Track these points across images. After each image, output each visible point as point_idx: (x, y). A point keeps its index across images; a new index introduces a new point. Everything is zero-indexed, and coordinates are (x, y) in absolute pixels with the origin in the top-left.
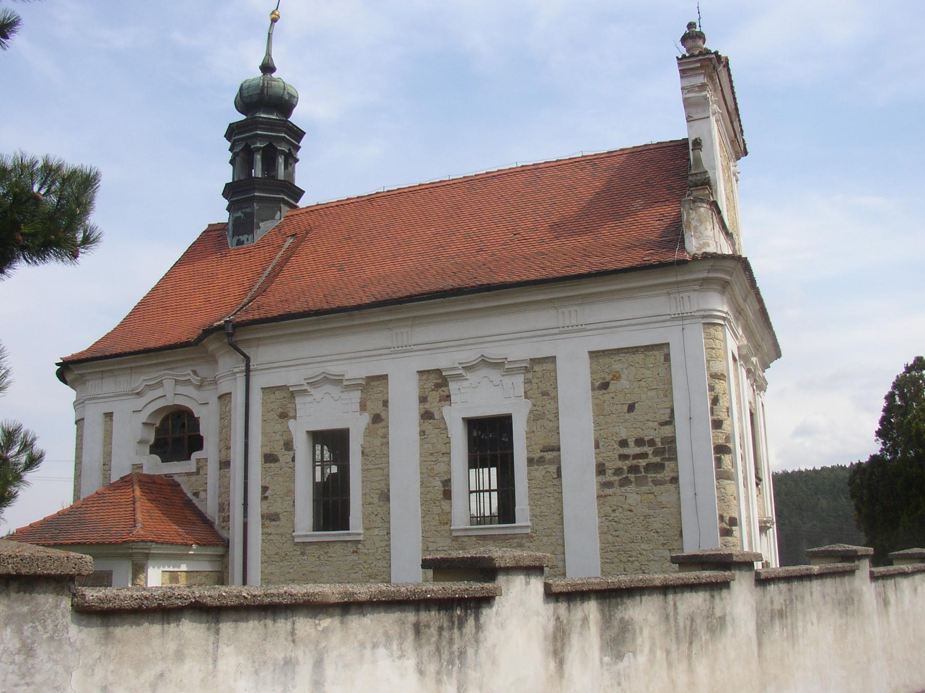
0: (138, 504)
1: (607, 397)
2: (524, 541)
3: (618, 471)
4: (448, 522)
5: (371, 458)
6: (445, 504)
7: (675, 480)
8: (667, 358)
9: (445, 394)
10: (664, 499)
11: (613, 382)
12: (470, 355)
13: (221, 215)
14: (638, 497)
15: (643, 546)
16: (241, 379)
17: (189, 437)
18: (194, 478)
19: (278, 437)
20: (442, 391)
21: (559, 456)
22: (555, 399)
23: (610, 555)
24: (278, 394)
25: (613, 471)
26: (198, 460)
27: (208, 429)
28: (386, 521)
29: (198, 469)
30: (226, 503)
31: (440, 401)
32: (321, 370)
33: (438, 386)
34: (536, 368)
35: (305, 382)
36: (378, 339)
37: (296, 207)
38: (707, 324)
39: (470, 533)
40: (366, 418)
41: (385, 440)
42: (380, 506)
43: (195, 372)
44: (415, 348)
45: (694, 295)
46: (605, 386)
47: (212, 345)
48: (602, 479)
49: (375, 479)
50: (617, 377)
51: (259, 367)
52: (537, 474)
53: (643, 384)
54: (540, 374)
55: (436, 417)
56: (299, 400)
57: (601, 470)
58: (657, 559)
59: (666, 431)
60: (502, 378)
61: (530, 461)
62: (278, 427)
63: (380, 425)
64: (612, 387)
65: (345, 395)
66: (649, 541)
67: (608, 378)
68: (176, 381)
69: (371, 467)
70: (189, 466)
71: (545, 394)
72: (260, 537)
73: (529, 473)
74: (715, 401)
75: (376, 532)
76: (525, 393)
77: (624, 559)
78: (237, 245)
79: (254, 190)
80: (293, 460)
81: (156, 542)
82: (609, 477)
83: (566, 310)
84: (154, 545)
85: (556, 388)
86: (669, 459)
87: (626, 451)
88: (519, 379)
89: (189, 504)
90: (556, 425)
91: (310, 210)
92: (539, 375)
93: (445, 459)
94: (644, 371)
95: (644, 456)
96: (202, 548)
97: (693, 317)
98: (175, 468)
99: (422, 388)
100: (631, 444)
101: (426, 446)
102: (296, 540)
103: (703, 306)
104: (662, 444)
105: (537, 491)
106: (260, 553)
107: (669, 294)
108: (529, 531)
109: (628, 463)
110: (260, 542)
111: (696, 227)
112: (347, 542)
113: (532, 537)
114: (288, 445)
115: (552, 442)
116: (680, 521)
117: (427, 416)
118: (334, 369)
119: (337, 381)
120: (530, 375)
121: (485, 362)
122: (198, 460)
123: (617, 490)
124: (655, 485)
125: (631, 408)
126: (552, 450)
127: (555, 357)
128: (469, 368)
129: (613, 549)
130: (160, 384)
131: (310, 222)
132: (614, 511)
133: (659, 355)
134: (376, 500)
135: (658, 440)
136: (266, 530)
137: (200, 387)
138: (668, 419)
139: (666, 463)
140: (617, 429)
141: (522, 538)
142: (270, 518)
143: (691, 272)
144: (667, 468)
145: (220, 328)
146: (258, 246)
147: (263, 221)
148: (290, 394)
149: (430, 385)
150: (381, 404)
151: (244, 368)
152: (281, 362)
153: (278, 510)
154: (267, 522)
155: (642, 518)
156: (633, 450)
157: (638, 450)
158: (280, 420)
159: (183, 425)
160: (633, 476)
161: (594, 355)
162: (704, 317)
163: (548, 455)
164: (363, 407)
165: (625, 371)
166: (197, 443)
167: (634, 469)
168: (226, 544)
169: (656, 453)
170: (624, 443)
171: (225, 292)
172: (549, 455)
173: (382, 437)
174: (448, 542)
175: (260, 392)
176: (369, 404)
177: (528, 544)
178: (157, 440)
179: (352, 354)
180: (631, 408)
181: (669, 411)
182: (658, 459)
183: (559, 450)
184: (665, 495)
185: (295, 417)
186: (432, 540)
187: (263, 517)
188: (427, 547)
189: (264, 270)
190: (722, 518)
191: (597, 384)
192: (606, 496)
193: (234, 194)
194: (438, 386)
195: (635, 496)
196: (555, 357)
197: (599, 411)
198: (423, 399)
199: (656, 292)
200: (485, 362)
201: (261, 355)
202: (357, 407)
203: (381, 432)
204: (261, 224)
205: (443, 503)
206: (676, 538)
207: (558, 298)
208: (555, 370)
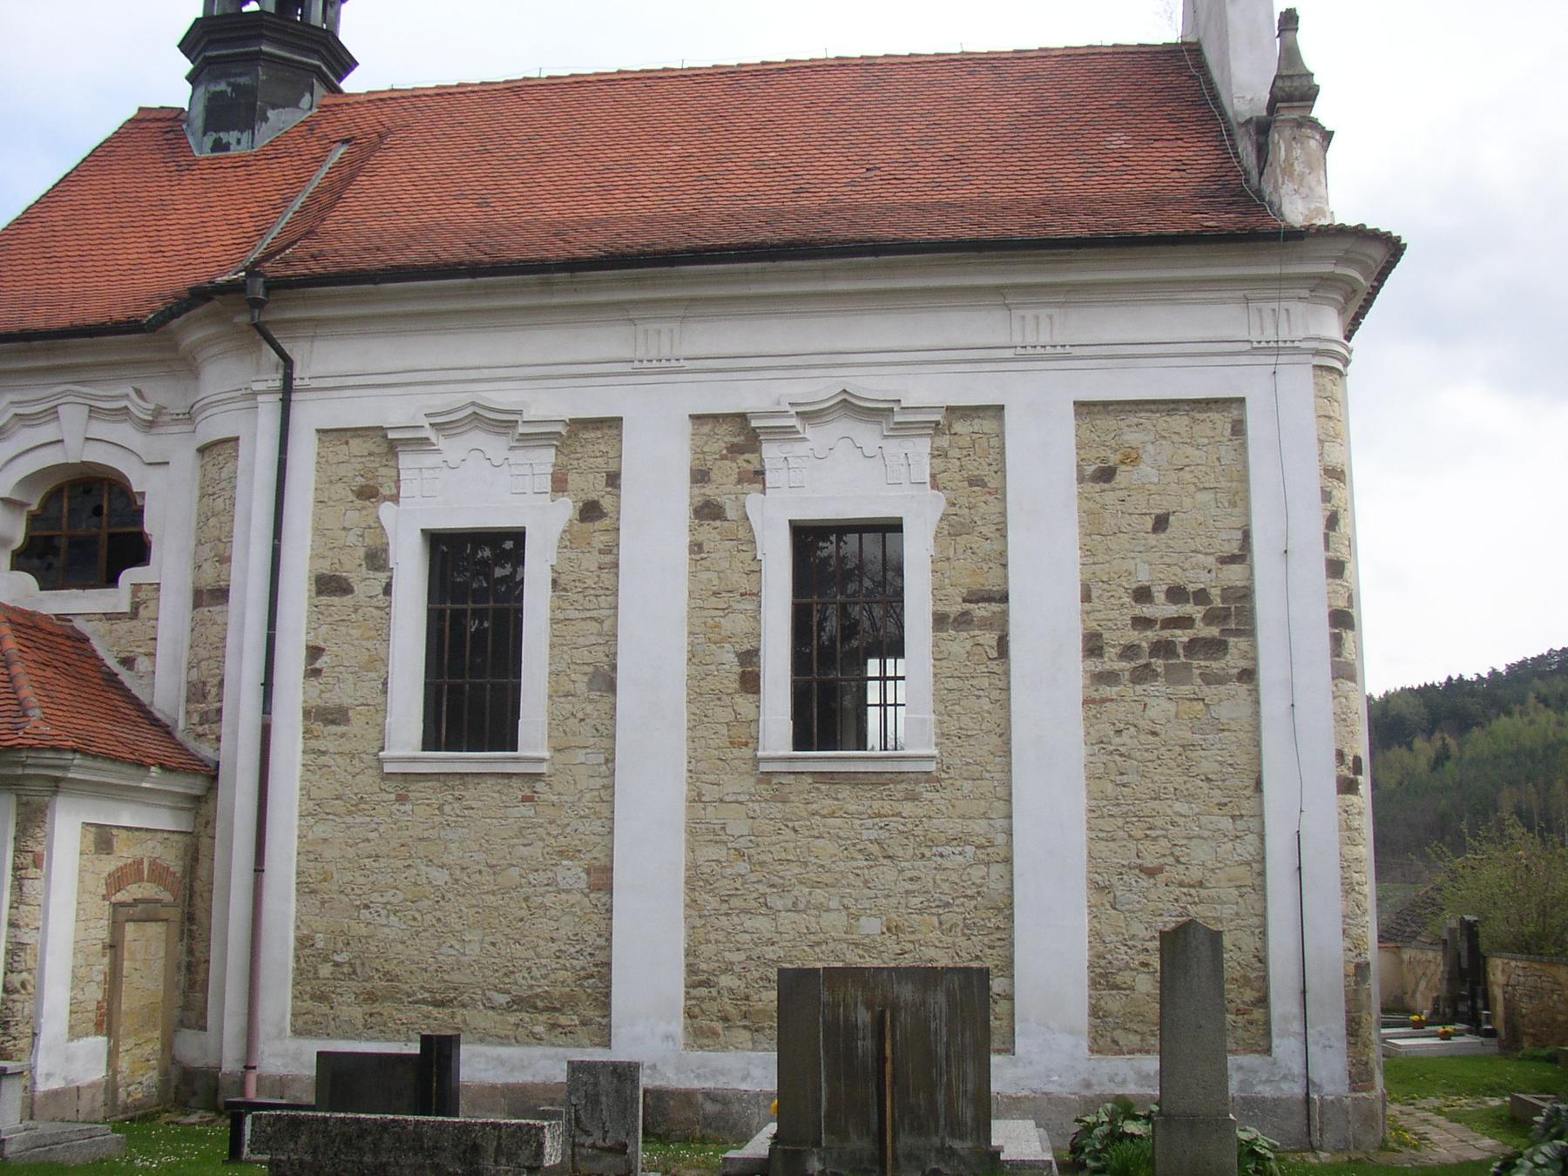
0: (18, 668)
1: (1110, 498)
2: (920, 788)
3: (1129, 651)
4: (753, 741)
5: (571, 596)
6: (743, 703)
7: (1248, 675)
8: (1239, 428)
9: (751, 467)
10: (1224, 712)
11: (1123, 467)
12: (818, 388)
13: (170, 83)
14: (1172, 707)
15: (1179, 807)
16: (268, 411)
17: (111, 536)
18: (124, 626)
19: (352, 539)
20: (745, 462)
21: (1005, 613)
22: (1000, 493)
23: (1108, 824)
24: (357, 446)
25: (1118, 650)
26: (137, 587)
27: (168, 516)
28: (607, 733)
29: (135, 608)
30: (215, 681)
31: (740, 481)
32: (464, 399)
33: (734, 450)
34: (959, 427)
35: (425, 422)
36: (604, 342)
37: (340, 91)
38: (1321, 367)
39: (799, 767)
40: (565, 509)
41: (608, 559)
42: (591, 701)
43: (139, 393)
44: (688, 365)
45: (1298, 308)
46: (1106, 474)
47: (193, 333)
48: (1098, 665)
49: (581, 641)
50: (1132, 459)
51: (315, 384)
52: (955, 647)
53: (1187, 476)
54: (968, 438)
55: (731, 513)
56: (406, 461)
57: (1093, 646)
58: (1206, 834)
59: (1233, 575)
60: (883, 443)
61: (940, 621)
62: (353, 517)
63: (598, 525)
64: (1121, 478)
65: (518, 456)
66: (1191, 797)
67: (1114, 459)
68: (92, 409)
69: (572, 614)
70: (116, 599)
71: (975, 482)
72: (299, 758)
73: (936, 645)
74: (1332, 522)
75: (580, 756)
76: (933, 476)
77: (1140, 834)
78: (213, 150)
79: (260, 38)
80: (387, 590)
81: (85, 754)
82: (1111, 662)
83: (1029, 314)
84: (78, 759)
85: (1001, 471)
86: (1238, 633)
87: (1147, 610)
88: (921, 448)
89: (112, 679)
90: (997, 547)
91: (357, 101)
92: (965, 441)
93: (748, 605)
94: (1190, 451)
95: (1184, 622)
96: (172, 776)
97: (1296, 351)
98: (77, 604)
99: (698, 452)
100: (1159, 596)
101: (704, 576)
102: (388, 768)
103: (1313, 332)
104: (1224, 601)
105: (952, 683)
106: (297, 793)
107: (1247, 300)
108: (931, 767)
109: (1151, 635)
110: (299, 770)
111: (1302, 176)
112: (509, 775)
113: (939, 780)
114: (377, 559)
115: (990, 583)
116: (1258, 757)
117: (707, 511)
118: (501, 397)
119: (503, 424)
120: (944, 442)
121: (848, 406)
122: (137, 587)
123: (1126, 689)
124: (1208, 683)
125: (1161, 523)
126: (988, 598)
127: (1002, 407)
128: (809, 417)
129: (1115, 810)
130: (52, 414)
131: (383, 119)
132: (1119, 732)
133: (1221, 422)
134: (581, 687)
135: (1215, 593)
136: (314, 744)
137: (150, 425)
138: (1236, 551)
139: (1232, 640)
140: (1130, 564)
141: (917, 782)
142: (323, 716)
143: (1301, 260)
144: (1232, 650)
145: (233, 289)
146: (263, 156)
147: (274, 107)
148: (390, 445)
149: (718, 446)
150: (601, 480)
151: (278, 384)
152: (363, 376)
153: (347, 701)
154: (318, 727)
155: (1178, 749)
156: (1162, 609)
157: (1172, 610)
158: (359, 503)
159: (98, 511)
160: (1160, 662)
161: (1085, 410)
162: (1317, 353)
163: (981, 610)
164: (559, 484)
165: (1150, 448)
166: (135, 550)
167: (1163, 649)
168: (211, 774)
169: (1210, 618)
170: (1143, 595)
171: (211, 232)
172: (980, 611)
173: (601, 552)
174: (749, 783)
175: (314, 437)
176: (574, 480)
177: (929, 795)
178: (30, 540)
179: (545, 366)
180: (1161, 523)
181: (1239, 535)
182: (1214, 631)
183: (1004, 598)
184: (1228, 704)
185: (395, 499)
186: (712, 778)
187: (307, 714)
188: (700, 795)
189: (288, 200)
190: (1340, 755)
191: (1090, 470)
192: (1103, 701)
193: (212, 43)
194: (734, 450)
195: (1165, 704)
196: (1002, 407)
197: (1093, 526)
198: (700, 476)
199: (1225, 295)
200: (848, 406)
201: (318, 359)
202: (547, 484)
203: (600, 540)
204: (270, 113)
205: (739, 699)
206: (1248, 793)
207: (1015, 287)
208: (1001, 435)
